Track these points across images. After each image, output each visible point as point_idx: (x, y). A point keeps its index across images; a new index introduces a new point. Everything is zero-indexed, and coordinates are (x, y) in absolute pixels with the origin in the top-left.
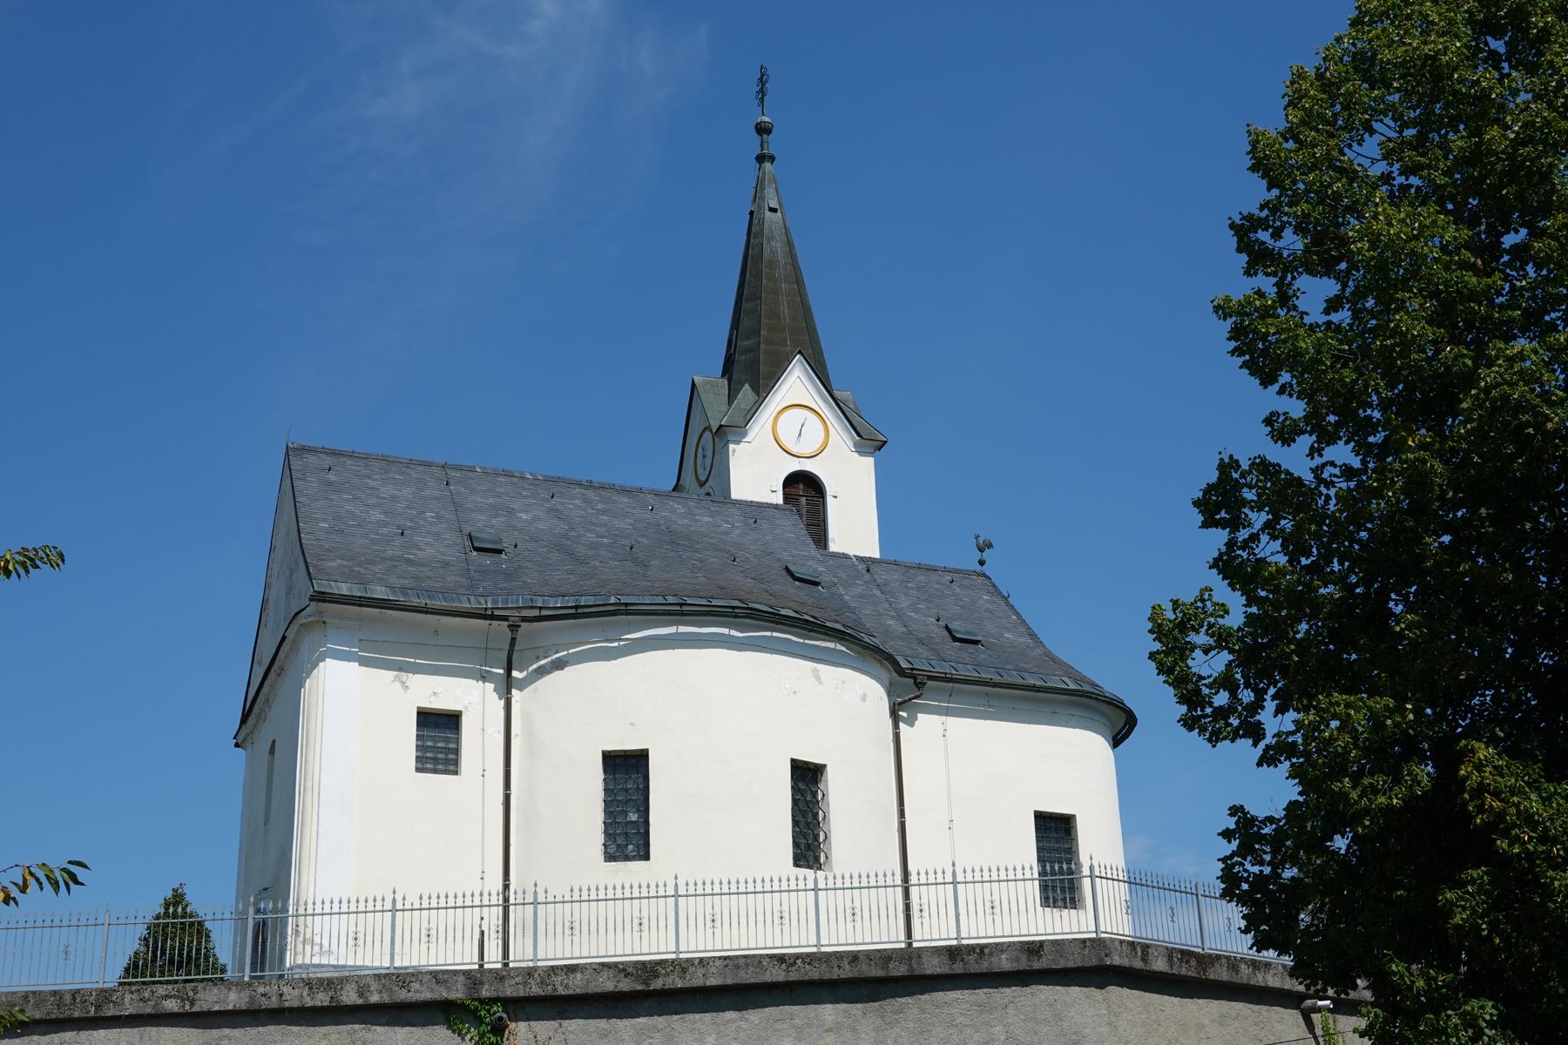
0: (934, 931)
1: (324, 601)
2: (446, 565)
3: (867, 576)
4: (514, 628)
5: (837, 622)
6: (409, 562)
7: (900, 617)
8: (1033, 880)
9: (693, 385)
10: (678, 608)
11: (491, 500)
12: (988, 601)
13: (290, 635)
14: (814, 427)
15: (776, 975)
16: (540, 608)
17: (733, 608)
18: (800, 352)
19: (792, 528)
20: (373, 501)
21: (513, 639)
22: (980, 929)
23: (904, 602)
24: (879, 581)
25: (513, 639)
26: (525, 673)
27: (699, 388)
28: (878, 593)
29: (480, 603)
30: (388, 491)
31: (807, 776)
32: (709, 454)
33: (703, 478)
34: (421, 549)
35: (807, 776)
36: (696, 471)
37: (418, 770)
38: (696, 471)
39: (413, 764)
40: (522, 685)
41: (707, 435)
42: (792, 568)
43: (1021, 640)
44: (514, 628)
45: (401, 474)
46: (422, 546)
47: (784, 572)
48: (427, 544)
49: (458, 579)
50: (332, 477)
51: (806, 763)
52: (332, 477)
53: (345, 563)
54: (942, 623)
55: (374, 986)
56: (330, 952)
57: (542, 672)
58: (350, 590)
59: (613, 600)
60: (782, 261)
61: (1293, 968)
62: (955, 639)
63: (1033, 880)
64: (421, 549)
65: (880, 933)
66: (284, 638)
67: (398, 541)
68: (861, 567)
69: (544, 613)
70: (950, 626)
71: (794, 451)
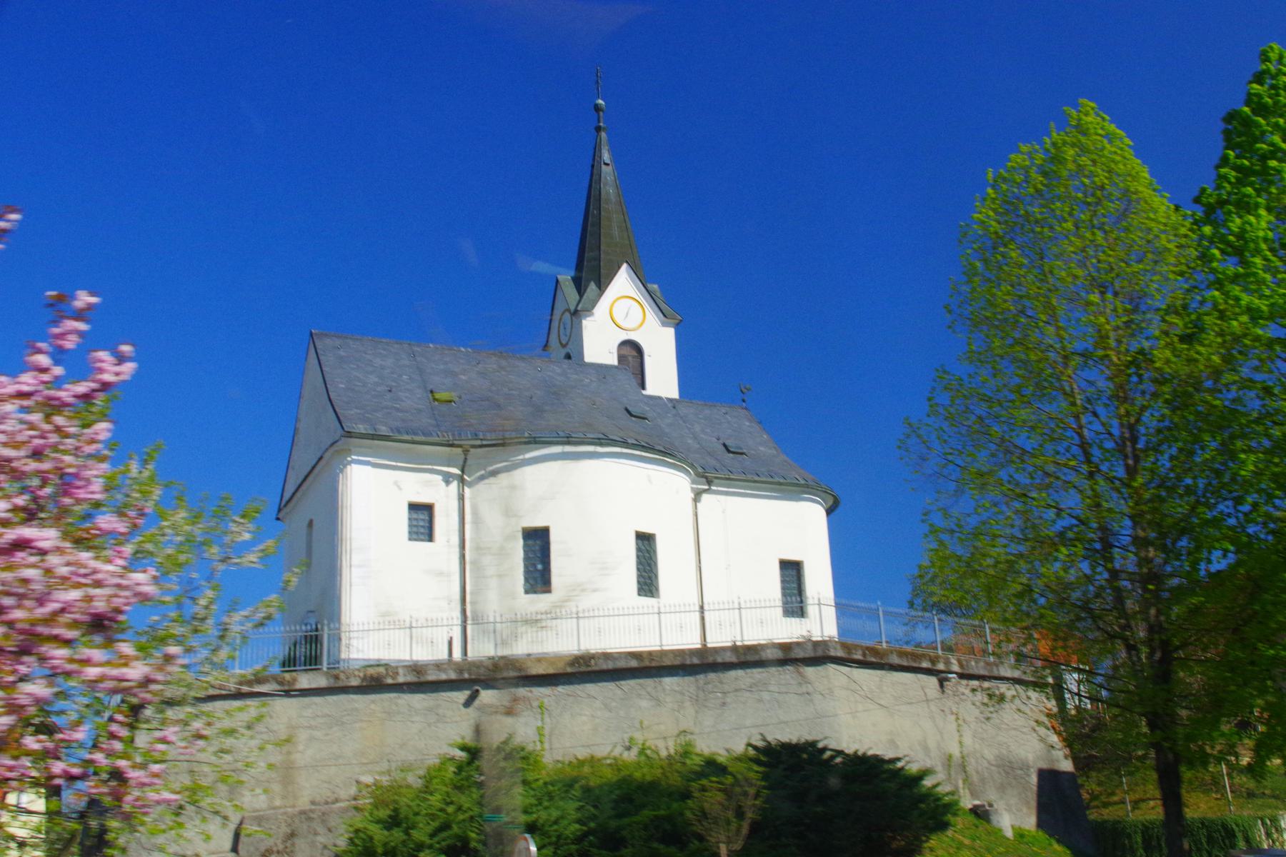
0: (720, 637)
1: (351, 437)
2: (419, 411)
3: (674, 411)
4: (466, 452)
5: (660, 445)
6: (398, 410)
7: (695, 438)
8: (733, 609)
9: (557, 281)
10: (566, 439)
11: (442, 367)
12: (749, 426)
13: (327, 455)
14: (636, 311)
15: (634, 664)
16: (481, 440)
17: (599, 439)
18: (627, 262)
19: (629, 382)
20: (370, 369)
21: (466, 459)
22: (753, 636)
23: (697, 428)
24: (682, 415)
25: (466, 459)
26: (473, 478)
27: (562, 284)
28: (681, 422)
29: (444, 436)
30: (378, 361)
31: (645, 541)
32: (568, 326)
33: (564, 342)
34: (403, 401)
35: (645, 541)
36: (559, 336)
37: (410, 539)
38: (559, 336)
39: (406, 535)
40: (470, 485)
41: (567, 315)
42: (630, 409)
43: (770, 451)
44: (466, 452)
45: (384, 350)
46: (404, 399)
47: (625, 412)
48: (406, 397)
49: (429, 421)
50: (342, 353)
51: (644, 533)
52: (342, 353)
53: (358, 411)
54: (721, 441)
55: (401, 671)
56: (363, 651)
57: (482, 478)
58: (365, 429)
59: (526, 435)
60: (614, 200)
61: (945, 814)
62: (729, 451)
63: (733, 609)
64: (403, 401)
65: (687, 639)
66: (321, 458)
67: (389, 396)
68: (670, 405)
69: (485, 443)
70: (727, 444)
71: (620, 322)
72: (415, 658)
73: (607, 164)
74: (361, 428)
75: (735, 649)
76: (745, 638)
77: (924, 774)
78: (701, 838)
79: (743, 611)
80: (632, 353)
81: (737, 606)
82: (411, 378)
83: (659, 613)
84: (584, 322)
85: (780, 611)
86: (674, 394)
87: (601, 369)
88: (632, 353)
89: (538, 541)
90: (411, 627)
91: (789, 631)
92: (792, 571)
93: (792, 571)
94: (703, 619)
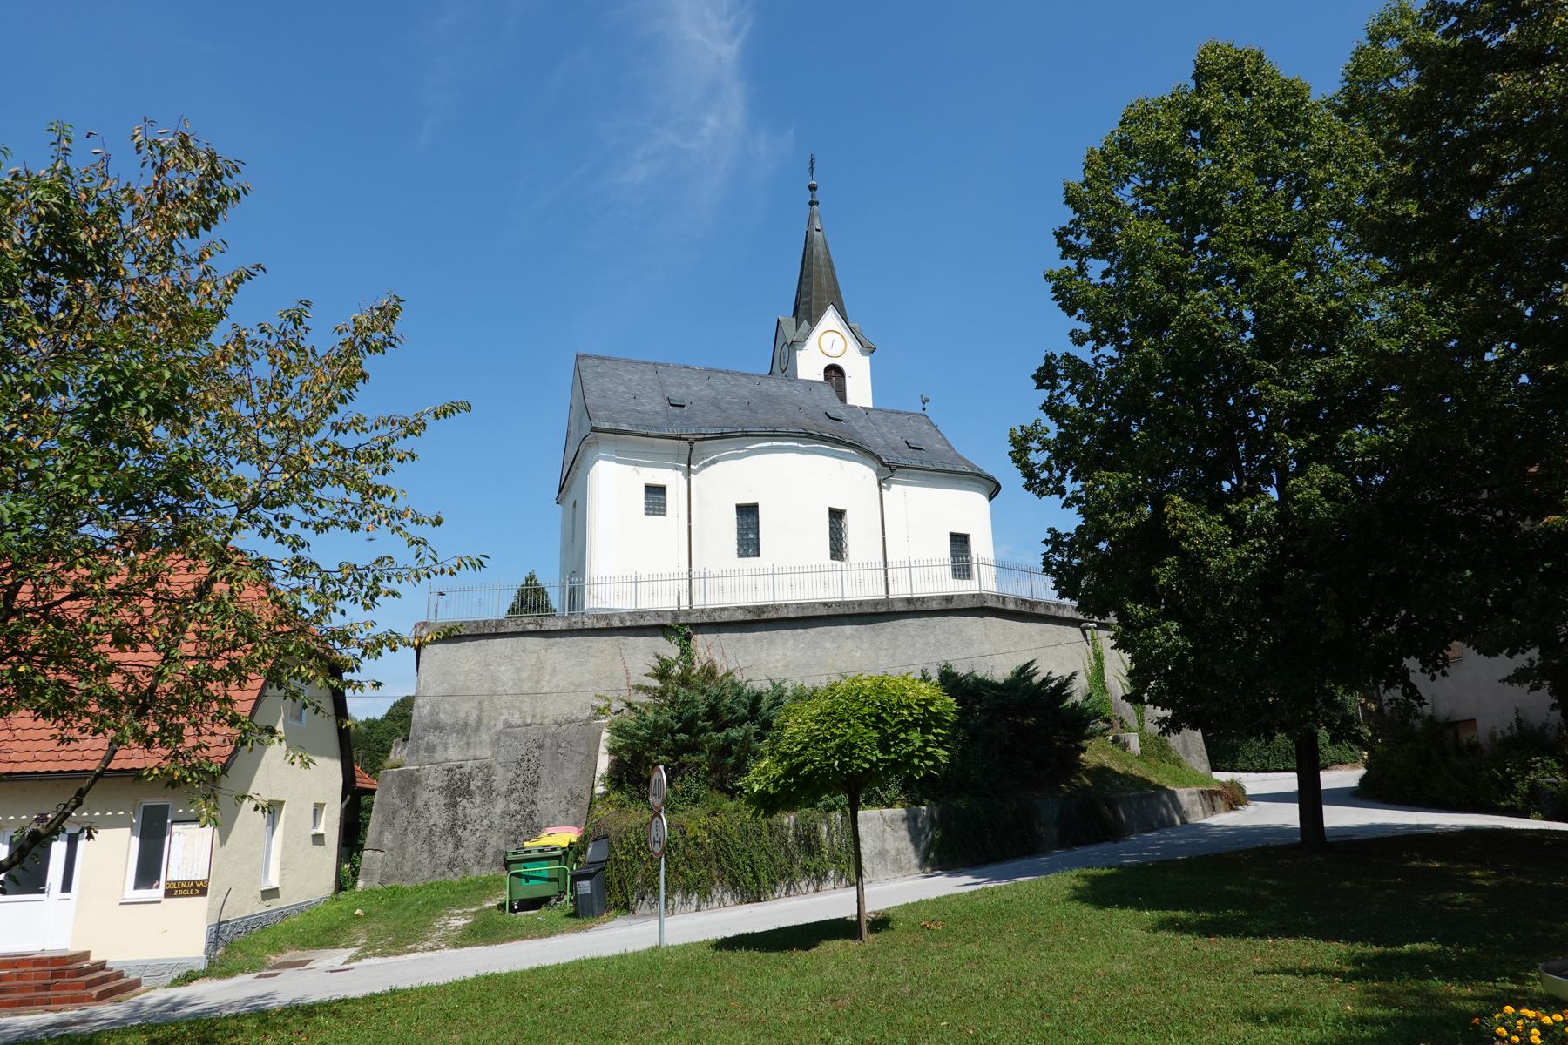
2: (657, 413)
4: (691, 444)
6: (638, 411)
7: (882, 436)
15: (823, 612)
19: (829, 392)
22: (923, 589)
23: (885, 429)
30: (627, 377)
31: (836, 515)
35: (836, 515)
37: (646, 514)
40: (696, 472)
44: (691, 444)
55: (628, 618)
57: (705, 465)
62: (910, 447)
67: (633, 402)
68: (864, 412)
72: (639, 607)
73: (818, 230)
74: (607, 425)
75: (909, 601)
76: (708, 602)
77: (1065, 683)
78: (1559, 730)
79: (707, 580)
80: (835, 373)
81: (633, 579)
82: (653, 390)
83: (636, 582)
84: (798, 352)
85: (949, 570)
86: (870, 404)
87: (810, 384)
88: (835, 373)
89: (748, 513)
90: (705, 578)
91: (950, 586)
92: (960, 542)
93: (960, 542)
94: (886, 574)
